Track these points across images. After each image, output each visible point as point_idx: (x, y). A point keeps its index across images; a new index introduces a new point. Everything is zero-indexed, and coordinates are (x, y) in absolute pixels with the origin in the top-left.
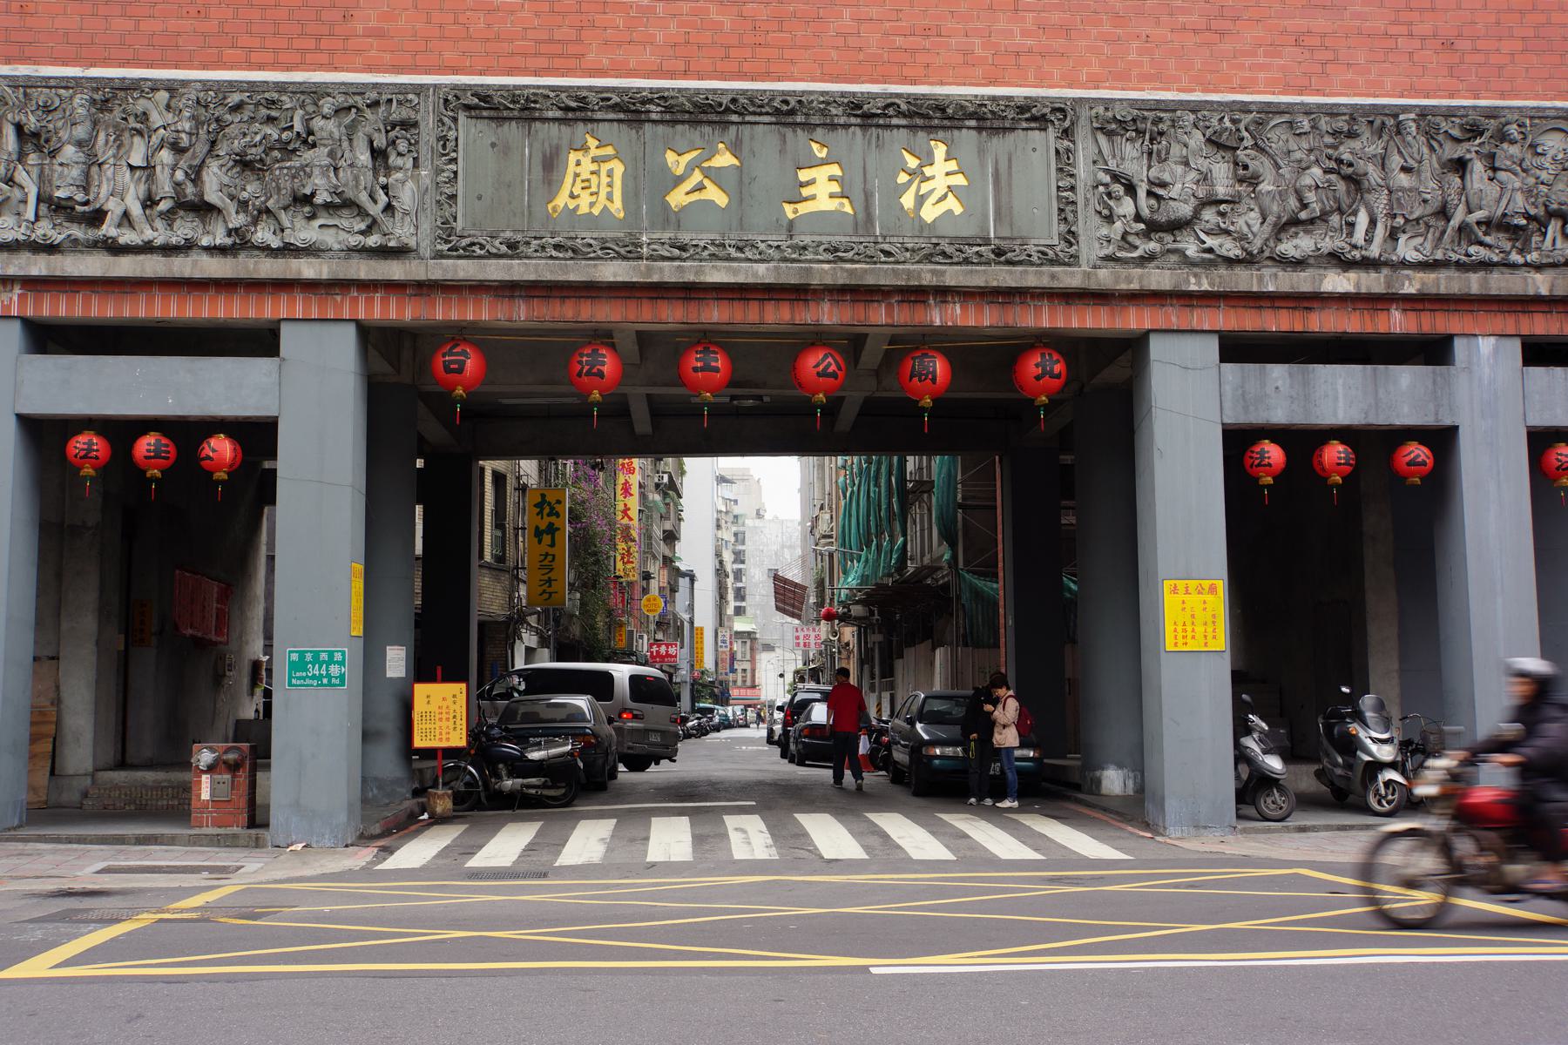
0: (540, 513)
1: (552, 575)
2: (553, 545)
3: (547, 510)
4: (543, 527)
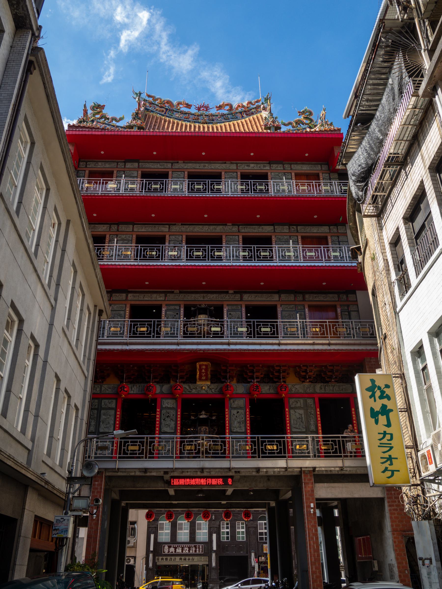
0: (373, 396)
1: (392, 453)
2: (389, 425)
3: (378, 394)
4: (377, 408)
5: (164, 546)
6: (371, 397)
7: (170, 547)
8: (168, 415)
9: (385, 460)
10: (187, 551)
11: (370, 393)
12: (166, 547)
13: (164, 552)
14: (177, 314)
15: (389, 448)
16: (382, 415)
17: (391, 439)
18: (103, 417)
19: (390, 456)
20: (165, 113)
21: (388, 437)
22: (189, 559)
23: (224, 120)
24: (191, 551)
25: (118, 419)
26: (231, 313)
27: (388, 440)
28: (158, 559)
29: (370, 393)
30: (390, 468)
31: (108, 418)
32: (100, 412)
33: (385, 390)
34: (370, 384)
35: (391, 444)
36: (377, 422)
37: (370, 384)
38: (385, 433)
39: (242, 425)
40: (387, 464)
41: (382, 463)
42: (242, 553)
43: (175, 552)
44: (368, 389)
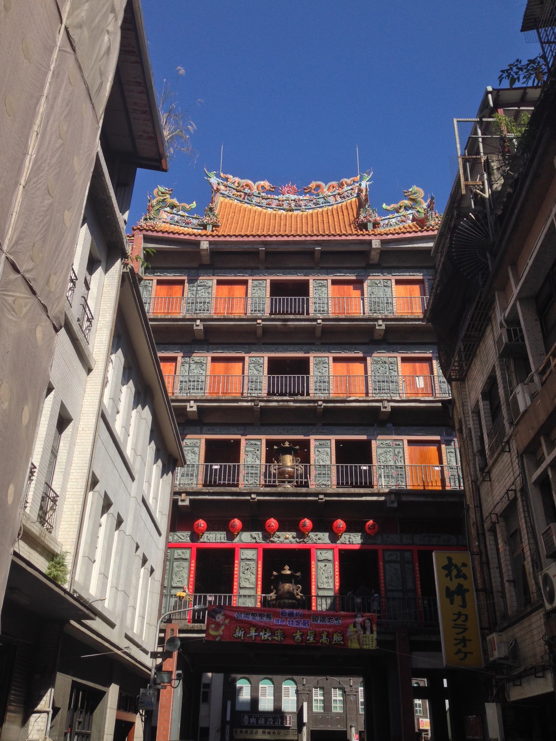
2: (464, 606)
3: (454, 572)
5: (243, 716)
6: (447, 576)
7: (250, 717)
8: (247, 567)
9: (458, 641)
10: (272, 723)
11: (446, 572)
12: (246, 717)
13: (243, 723)
14: (258, 450)
15: (462, 630)
16: (458, 595)
17: (466, 620)
18: (176, 569)
19: (464, 638)
20: (244, 199)
21: (463, 618)
22: (274, 733)
23: (313, 206)
24: (276, 723)
25: (192, 572)
26: (319, 450)
27: (463, 621)
28: (236, 732)
29: (446, 572)
30: (464, 650)
31: (181, 571)
32: (173, 563)
33: (462, 568)
34: (447, 563)
35: (465, 625)
36: (452, 602)
37: (447, 563)
38: (459, 614)
39: (331, 581)
40: (460, 646)
41: (456, 645)
42: (339, 728)
43: (257, 723)
44: (444, 568)
